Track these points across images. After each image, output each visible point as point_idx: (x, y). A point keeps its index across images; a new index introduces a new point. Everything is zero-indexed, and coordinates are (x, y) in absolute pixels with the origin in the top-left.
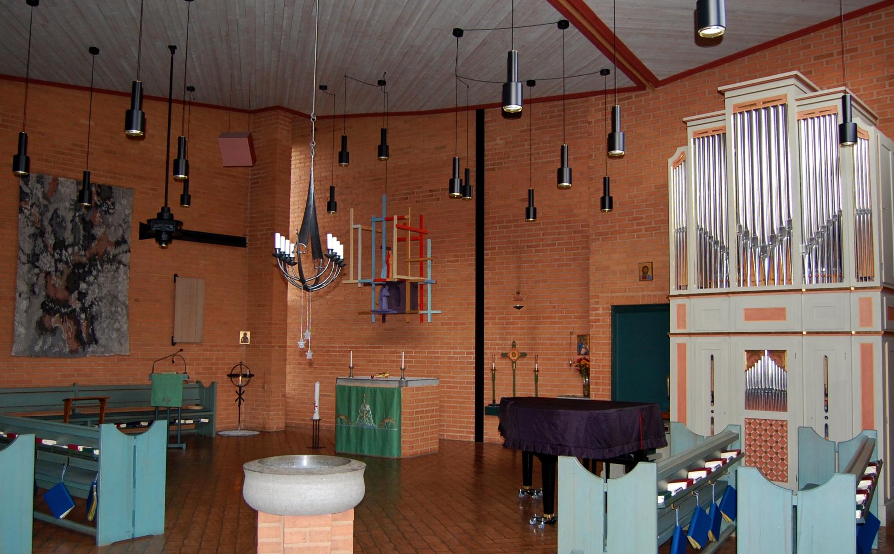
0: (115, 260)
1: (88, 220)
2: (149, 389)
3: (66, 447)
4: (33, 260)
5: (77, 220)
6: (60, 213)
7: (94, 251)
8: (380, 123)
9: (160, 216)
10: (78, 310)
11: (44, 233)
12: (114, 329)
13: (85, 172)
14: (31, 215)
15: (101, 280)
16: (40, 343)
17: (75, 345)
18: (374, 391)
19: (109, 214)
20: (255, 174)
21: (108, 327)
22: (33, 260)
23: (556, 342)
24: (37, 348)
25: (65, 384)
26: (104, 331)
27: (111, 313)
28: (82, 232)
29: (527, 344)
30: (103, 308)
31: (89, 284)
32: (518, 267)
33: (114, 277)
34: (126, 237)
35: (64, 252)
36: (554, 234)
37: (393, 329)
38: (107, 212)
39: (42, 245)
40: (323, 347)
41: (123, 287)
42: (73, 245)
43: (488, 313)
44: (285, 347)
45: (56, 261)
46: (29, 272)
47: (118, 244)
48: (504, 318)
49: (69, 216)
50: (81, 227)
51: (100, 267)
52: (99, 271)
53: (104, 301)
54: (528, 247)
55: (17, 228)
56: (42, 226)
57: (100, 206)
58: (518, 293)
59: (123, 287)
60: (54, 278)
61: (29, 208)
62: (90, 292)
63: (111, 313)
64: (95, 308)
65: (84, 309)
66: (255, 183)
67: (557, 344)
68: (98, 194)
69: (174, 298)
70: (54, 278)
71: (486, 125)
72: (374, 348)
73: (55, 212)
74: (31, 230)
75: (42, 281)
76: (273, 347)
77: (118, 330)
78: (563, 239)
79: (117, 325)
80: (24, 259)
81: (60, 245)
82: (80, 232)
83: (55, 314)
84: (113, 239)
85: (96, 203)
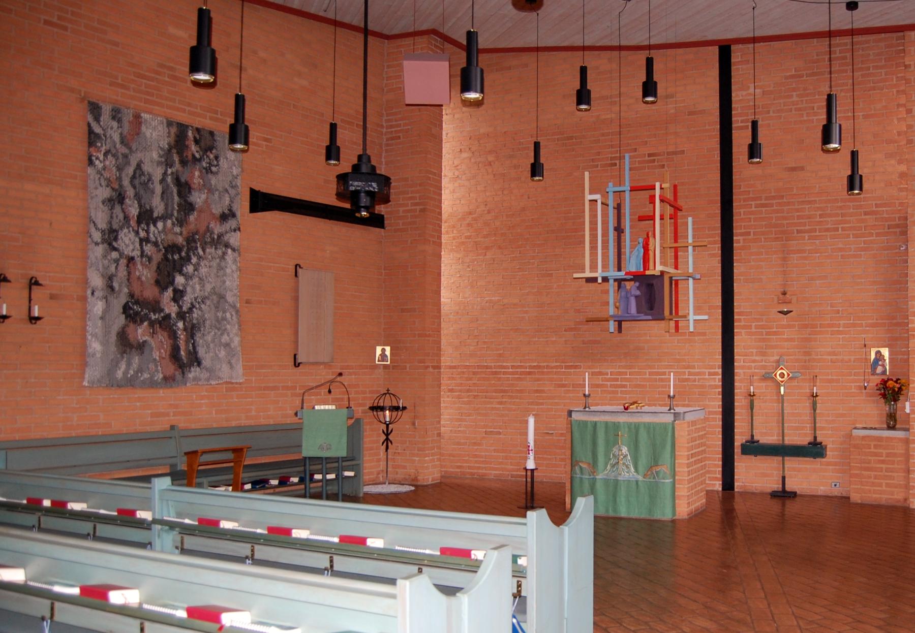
0: (219, 242)
1: (183, 180)
2: (299, 429)
3: (25, 502)
4: (111, 237)
5: (169, 179)
6: (146, 168)
7: (192, 227)
8: (577, 60)
9: (356, 168)
10: (173, 315)
11: (123, 198)
12: (221, 344)
13: (237, 96)
14: (104, 168)
15: (203, 270)
16: (123, 366)
17: (171, 369)
18: (635, 429)
19: (212, 172)
20: (392, 127)
21: (213, 341)
22: (111, 237)
23: (840, 357)
24: (120, 374)
25: (157, 428)
26: (208, 347)
27: (218, 320)
28: (176, 198)
29: (797, 360)
30: (206, 313)
31: (188, 277)
32: (784, 259)
33: (220, 268)
34: (234, 209)
35: (152, 228)
36: (837, 215)
37: (595, 342)
38: (208, 170)
39: (121, 216)
40: (487, 367)
41: (232, 282)
42: (164, 218)
43: (740, 320)
44: (439, 367)
45: (141, 240)
46: (105, 257)
47: (224, 217)
48: (762, 327)
49: (157, 173)
50: (175, 190)
51: (201, 252)
52: (199, 258)
53: (208, 302)
54: (798, 232)
55: (85, 188)
56: (121, 186)
57: (200, 160)
58: (784, 293)
59: (232, 282)
60: (139, 267)
61: (101, 158)
62: (189, 289)
63: (218, 320)
64: (196, 314)
65: (181, 315)
66: (392, 139)
67: (842, 361)
68: (197, 142)
69: (296, 299)
70: (139, 267)
71: (733, 68)
72: (566, 367)
73: (139, 166)
74: (105, 193)
75: (122, 272)
76: (427, 367)
77: (227, 345)
78: (849, 222)
79: (225, 339)
80: (97, 236)
81: (146, 217)
82: (173, 199)
83: (142, 322)
84: (217, 210)
85: (193, 156)
